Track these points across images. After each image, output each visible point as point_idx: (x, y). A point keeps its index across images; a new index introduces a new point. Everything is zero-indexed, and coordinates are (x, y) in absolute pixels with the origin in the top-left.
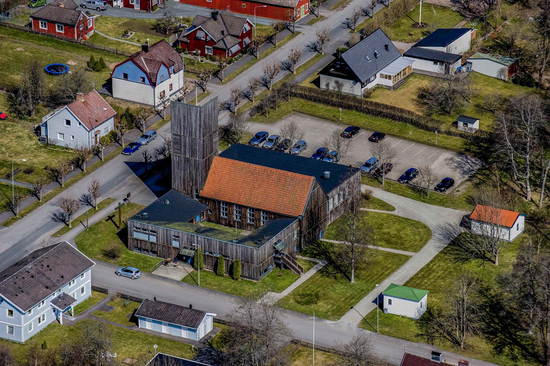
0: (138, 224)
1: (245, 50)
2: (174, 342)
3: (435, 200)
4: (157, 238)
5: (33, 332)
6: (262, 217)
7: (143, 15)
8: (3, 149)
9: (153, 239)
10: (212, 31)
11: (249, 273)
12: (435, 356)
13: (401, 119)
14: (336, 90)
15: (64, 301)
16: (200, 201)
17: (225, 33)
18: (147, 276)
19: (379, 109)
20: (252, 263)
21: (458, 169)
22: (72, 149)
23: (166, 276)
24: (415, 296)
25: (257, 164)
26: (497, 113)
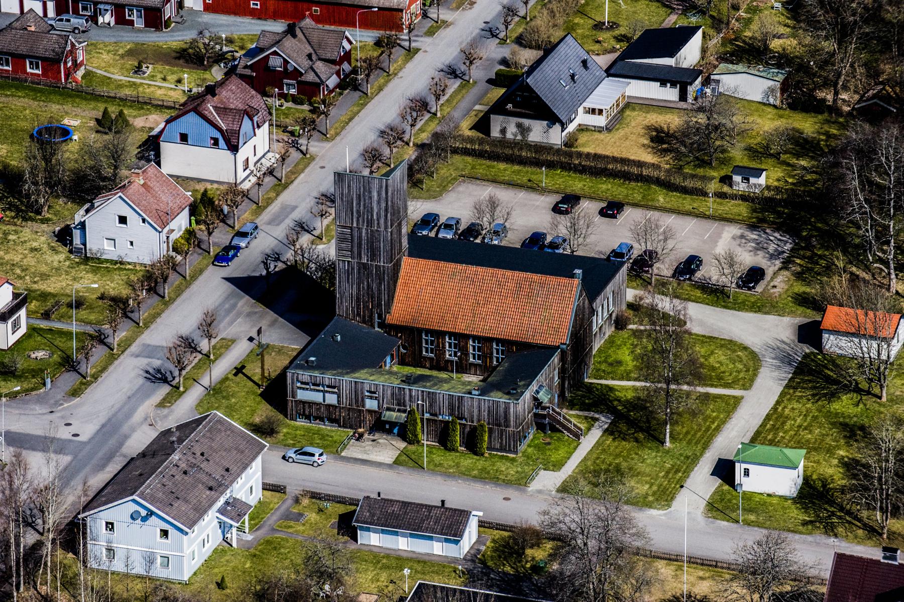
0: (305, 376)
1: (349, 83)
2: (425, 562)
3: (743, 303)
4: (339, 397)
5: (197, 563)
6: (495, 351)
7: (151, 35)
8: (18, 271)
9: (332, 399)
10: (294, 53)
11: (501, 443)
12: (888, 554)
13: (640, 178)
14: (519, 137)
15: (234, 509)
16: (385, 332)
17: (314, 57)
18: (336, 459)
19: (600, 165)
20: (508, 426)
21: (759, 252)
22: (129, 263)
23: (365, 457)
24: (790, 461)
25: (477, 265)
26: (783, 157)
